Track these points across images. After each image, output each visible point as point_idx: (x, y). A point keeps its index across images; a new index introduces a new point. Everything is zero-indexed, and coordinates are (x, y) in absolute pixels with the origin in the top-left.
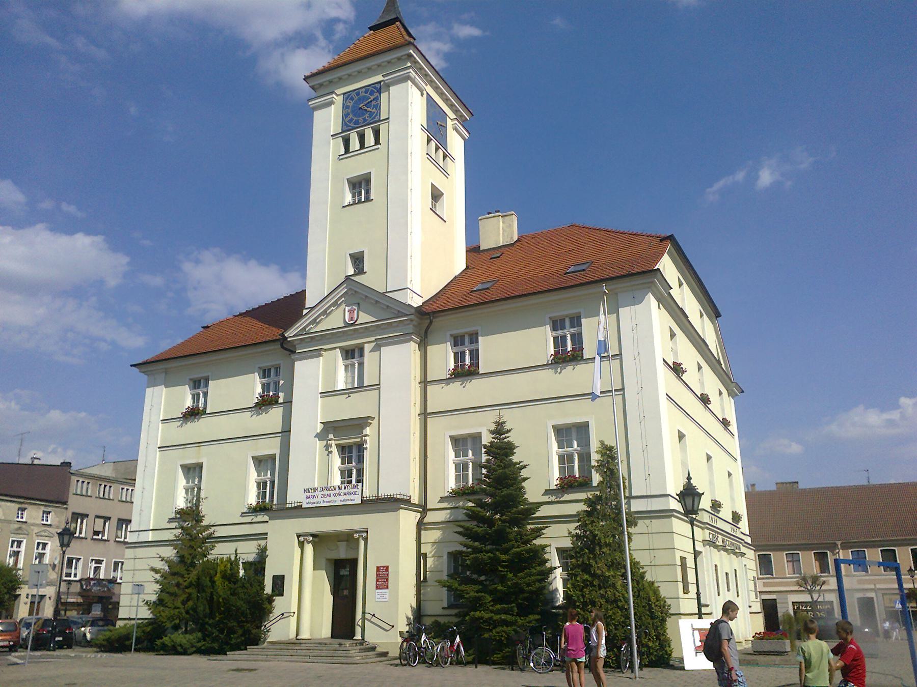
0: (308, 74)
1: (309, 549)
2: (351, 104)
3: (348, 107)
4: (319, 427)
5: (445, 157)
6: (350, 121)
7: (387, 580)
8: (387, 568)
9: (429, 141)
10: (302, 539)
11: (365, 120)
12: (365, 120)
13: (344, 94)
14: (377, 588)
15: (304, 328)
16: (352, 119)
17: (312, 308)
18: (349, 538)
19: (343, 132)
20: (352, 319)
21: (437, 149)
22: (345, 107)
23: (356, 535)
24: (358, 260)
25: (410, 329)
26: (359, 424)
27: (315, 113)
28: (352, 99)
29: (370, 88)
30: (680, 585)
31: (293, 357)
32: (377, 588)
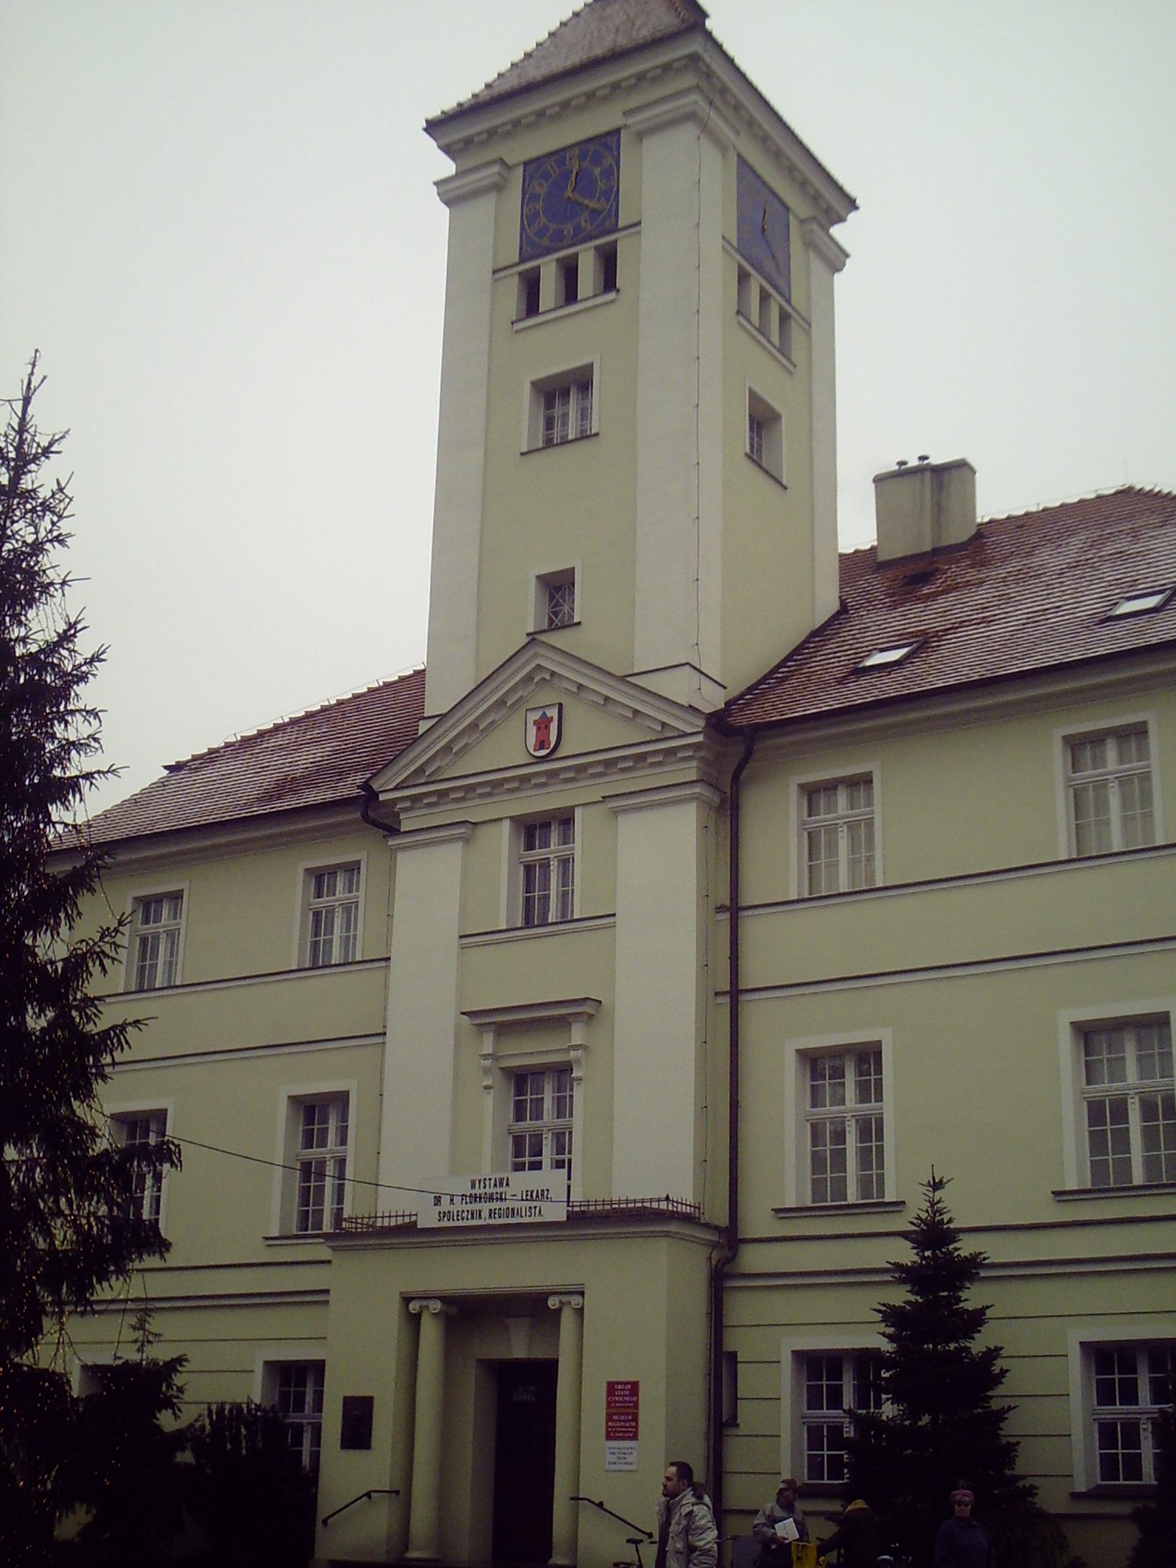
0: (435, 112)
1: (430, 1331)
2: (541, 189)
3: (534, 198)
4: (425, 125)
5: (784, 318)
6: (541, 233)
7: (635, 1418)
8: (634, 1387)
9: (743, 277)
10: (414, 1307)
11: (578, 228)
12: (578, 228)
13: (520, 273)
14: (610, 1436)
15: (421, 770)
16: (546, 228)
17: (442, 717)
18: (535, 1309)
19: (523, 260)
20: (541, 745)
21: (764, 297)
22: (528, 197)
23: (553, 1302)
24: (557, 588)
25: (690, 771)
26: (554, 1018)
27: (454, 172)
28: (546, 176)
29: (592, 147)
30: (349, 1173)
31: (392, 842)
32: (610, 1436)
